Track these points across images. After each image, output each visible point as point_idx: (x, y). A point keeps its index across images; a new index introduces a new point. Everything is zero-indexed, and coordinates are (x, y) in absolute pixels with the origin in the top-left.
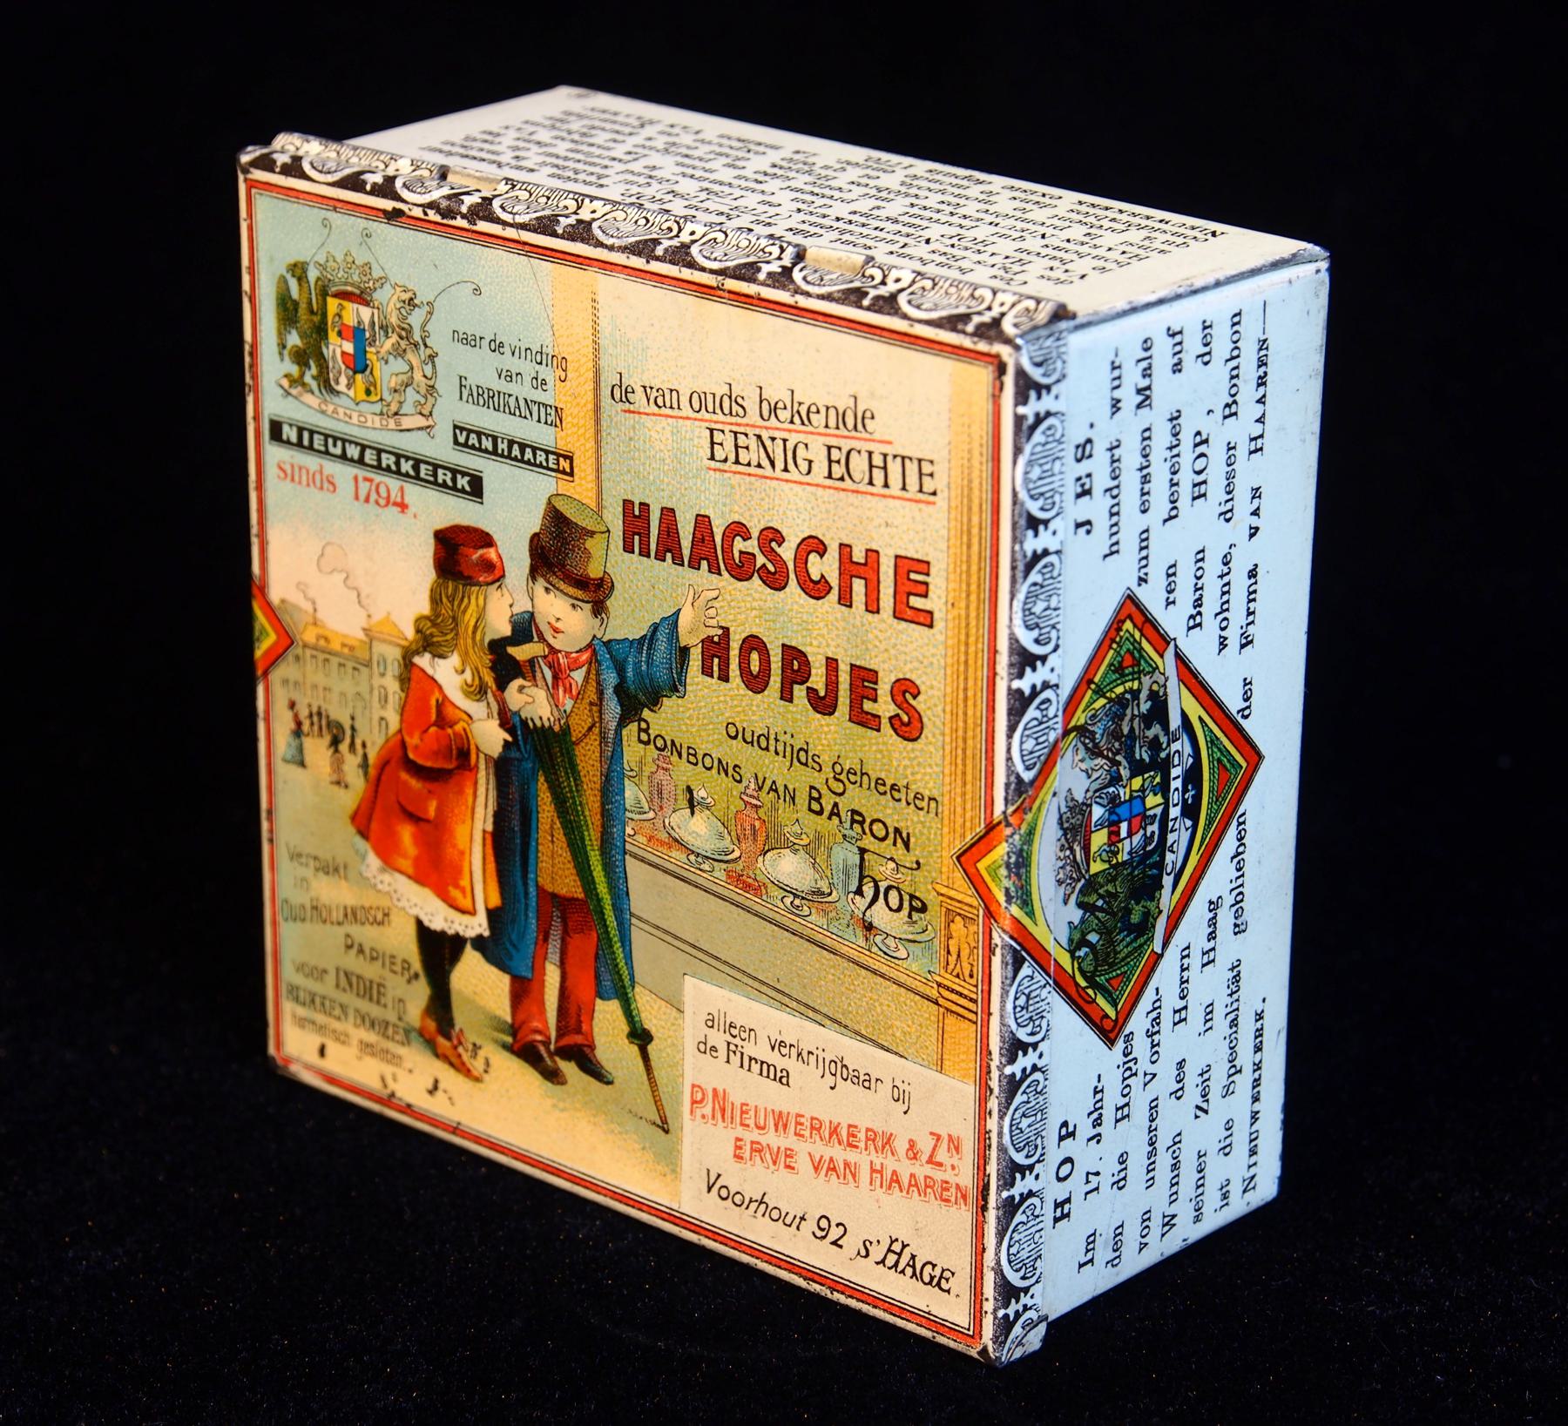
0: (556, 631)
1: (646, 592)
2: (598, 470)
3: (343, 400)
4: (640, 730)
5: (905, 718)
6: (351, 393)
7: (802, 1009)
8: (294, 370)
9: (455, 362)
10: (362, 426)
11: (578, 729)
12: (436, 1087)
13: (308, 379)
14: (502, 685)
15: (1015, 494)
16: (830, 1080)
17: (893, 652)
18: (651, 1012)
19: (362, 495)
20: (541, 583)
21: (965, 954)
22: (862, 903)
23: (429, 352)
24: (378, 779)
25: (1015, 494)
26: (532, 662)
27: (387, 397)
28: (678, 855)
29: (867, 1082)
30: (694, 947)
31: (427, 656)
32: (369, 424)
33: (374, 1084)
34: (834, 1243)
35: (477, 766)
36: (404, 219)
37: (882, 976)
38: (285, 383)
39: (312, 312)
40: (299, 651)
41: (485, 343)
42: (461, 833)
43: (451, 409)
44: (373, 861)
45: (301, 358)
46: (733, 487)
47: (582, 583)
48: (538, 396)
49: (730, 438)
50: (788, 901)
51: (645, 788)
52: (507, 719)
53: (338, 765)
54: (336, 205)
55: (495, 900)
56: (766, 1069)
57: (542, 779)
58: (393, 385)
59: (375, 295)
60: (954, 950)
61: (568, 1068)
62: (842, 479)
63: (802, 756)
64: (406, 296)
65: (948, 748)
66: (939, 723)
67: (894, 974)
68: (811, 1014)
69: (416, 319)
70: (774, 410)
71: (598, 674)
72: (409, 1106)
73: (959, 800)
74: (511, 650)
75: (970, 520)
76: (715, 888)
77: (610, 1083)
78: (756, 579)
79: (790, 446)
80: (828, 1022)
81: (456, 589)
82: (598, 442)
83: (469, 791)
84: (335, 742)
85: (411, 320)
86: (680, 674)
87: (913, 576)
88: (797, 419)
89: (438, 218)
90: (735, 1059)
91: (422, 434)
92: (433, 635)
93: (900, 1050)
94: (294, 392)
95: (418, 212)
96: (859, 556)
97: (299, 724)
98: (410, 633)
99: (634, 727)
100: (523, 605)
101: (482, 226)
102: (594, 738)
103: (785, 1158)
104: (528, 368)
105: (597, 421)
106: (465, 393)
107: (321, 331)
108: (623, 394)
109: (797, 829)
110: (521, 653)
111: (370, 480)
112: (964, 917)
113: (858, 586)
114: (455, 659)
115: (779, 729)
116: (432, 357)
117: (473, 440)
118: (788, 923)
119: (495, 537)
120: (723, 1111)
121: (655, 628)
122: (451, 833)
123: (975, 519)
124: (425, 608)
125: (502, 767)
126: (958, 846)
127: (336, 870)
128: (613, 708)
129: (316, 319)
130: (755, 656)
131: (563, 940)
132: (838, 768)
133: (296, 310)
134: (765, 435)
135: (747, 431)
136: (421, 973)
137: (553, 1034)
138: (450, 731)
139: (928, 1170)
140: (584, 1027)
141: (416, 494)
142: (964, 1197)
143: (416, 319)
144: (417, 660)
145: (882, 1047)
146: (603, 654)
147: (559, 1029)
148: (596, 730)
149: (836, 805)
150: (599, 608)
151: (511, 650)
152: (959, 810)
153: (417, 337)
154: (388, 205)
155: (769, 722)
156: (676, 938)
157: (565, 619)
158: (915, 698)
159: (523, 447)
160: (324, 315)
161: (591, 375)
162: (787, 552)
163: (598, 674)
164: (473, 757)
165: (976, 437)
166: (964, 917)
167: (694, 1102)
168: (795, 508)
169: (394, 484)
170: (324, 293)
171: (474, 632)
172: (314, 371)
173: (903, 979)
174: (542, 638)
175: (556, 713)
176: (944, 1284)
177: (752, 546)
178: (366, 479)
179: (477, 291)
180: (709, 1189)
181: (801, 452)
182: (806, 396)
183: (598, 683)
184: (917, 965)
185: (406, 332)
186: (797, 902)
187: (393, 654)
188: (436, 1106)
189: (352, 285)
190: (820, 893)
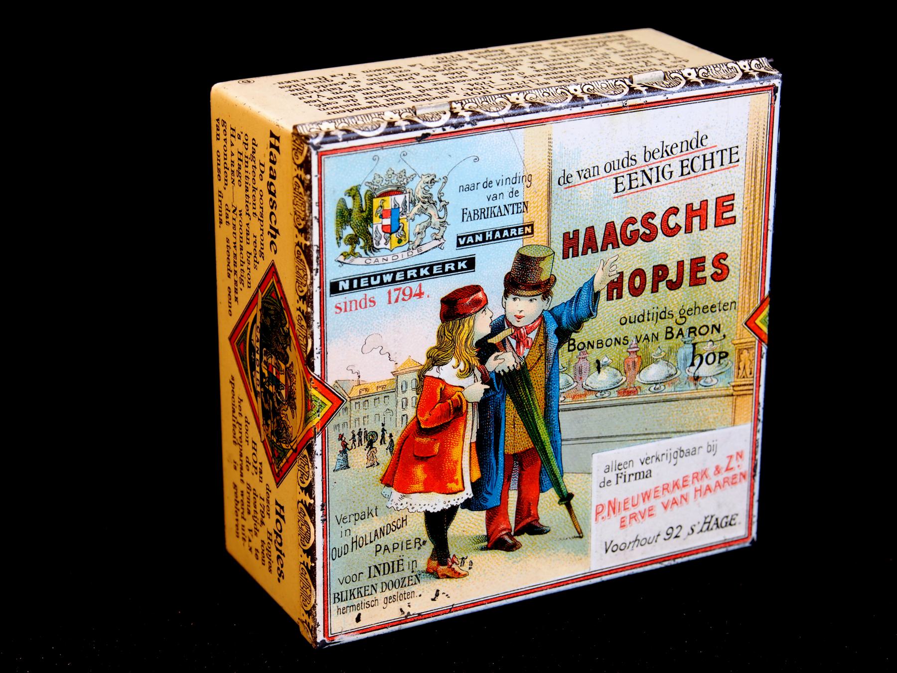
0: (519, 318)
1: (569, 276)
2: (549, 225)
3: (383, 252)
4: (569, 345)
5: (720, 271)
6: (388, 246)
7: (659, 436)
8: (348, 248)
9: (457, 201)
10: (394, 261)
11: (530, 363)
12: (437, 595)
13: (358, 249)
14: (483, 360)
15: (380, 135)
16: (674, 461)
17: (713, 244)
18: (570, 483)
19: (393, 299)
20: (511, 296)
21: (747, 367)
22: (693, 369)
23: (443, 203)
24: (400, 450)
25: (380, 135)
26: (503, 342)
27: (412, 239)
28: (591, 397)
29: (694, 452)
30: (598, 437)
31: (435, 368)
32: (400, 258)
33: (396, 615)
34: (676, 537)
35: (467, 412)
36: (430, 137)
37: (704, 398)
38: (342, 259)
39: (362, 211)
40: (347, 405)
41: (480, 186)
42: (455, 453)
43: (457, 227)
44: (396, 495)
46: (627, 201)
47: (537, 286)
48: (515, 200)
49: (627, 178)
50: (652, 389)
52: (485, 380)
54: (381, 146)
56: (639, 475)
58: (417, 230)
59: (407, 187)
60: (742, 367)
62: (689, 173)
63: (663, 315)
64: (429, 179)
65: (742, 276)
66: (737, 266)
67: (714, 393)
68: (664, 436)
69: (434, 190)
70: (652, 155)
71: (545, 328)
72: (419, 614)
73: (747, 296)
74: (489, 341)
75: (756, 166)
76: (614, 402)
78: (640, 241)
79: (660, 169)
80: (673, 435)
81: (454, 325)
82: (549, 210)
83: (461, 428)
84: (370, 444)
86: (593, 307)
87: (725, 204)
88: (665, 154)
89: (453, 129)
90: (621, 481)
92: (435, 360)
93: (712, 427)
94: (347, 261)
95: (440, 131)
96: (696, 206)
97: (345, 445)
98: (423, 360)
99: (566, 346)
100: (498, 313)
101: (481, 124)
102: (541, 364)
103: (650, 513)
104: (506, 189)
105: (549, 199)
106: (466, 217)
108: (566, 179)
109: (659, 351)
110: (494, 340)
111: (399, 289)
112: (747, 349)
113: (696, 221)
114: (454, 362)
115: (650, 308)
116: (444, 207)
117: (470, 239)
118: (656, 399)
120: (614, 509)
122: (449, 454)
123: (759, 165)
124: (434, 342)
125: (483, 406)
126: (746, 317)
127: (370, 513)
128: (553, 340)
129: (364, 214)
130: (638, 279)
131: (520, 475)
132: (682, 312)
133: (350, 215)
134: (647, 169)
135: (628, 173)
136: (428, 540)
137: (513, 526)
138: (449, 401)
139: (726, 474)
141: (428, 285)
142: (744, 477)
143: (434, 190)
144: (428, 373)
145: (703, 431)
146: (549, 318)
147: (516, 521)
148: (543, 358)
149: (681, 330)
150: (546, 295)
152: (747, 301)
153: (435, 198)
154: (419, 133)
155: (644, 307)
156: (588, 438)
157: (526, 309)
158: (725, 260)
159: (501, 231)
160: (371, 210)
161: (546, 177)
162: (657, 222)
163: (545, 328)
165: (762, 127)
166: (747, 349)
167: (597, 514)
168: (657, 200)
169: (414, 285)
170: (371, 198)
171: (466, 342)
172: (362, 243)
173: (718, 393)
174: (510, 325)
175: (518, 360)
176: (733, 522)
177: (638, 226)
178: (395, 290)
179: (477, 159)
180: (607, 551)
181: (667, 169)
182: (669, 142)
183: (545, 333)
184: (722, 384)
185: (428, 199)
186: (658, 386)
188: (442, 603)
189: (391, 186)
190: (671, 375)
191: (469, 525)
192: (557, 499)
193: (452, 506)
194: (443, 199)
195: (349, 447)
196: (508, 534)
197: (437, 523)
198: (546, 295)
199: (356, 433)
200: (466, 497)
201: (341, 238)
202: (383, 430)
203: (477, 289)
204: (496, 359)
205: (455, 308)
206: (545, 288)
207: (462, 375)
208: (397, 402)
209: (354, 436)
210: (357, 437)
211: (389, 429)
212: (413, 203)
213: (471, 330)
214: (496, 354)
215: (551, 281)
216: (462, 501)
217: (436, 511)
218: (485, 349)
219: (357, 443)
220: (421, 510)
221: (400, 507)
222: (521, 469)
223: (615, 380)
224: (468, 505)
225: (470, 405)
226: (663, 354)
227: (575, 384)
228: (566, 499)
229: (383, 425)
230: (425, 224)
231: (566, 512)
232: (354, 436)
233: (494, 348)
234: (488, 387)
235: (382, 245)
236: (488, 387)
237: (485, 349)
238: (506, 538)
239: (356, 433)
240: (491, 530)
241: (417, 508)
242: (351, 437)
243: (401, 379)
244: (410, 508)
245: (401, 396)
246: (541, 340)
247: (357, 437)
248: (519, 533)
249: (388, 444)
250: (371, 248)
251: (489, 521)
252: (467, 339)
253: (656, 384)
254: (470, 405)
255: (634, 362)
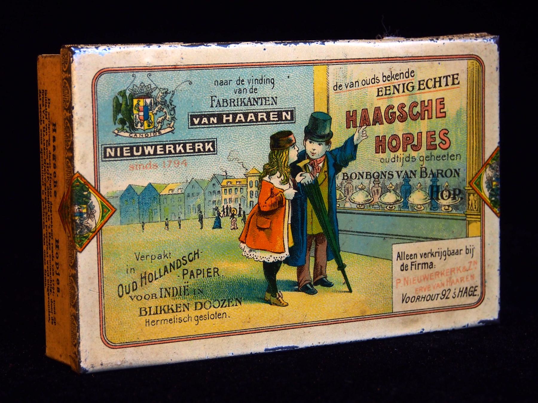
6: (143, 128)
8: (120, 126)
14: (294, 176)
23: (173, 106)
27: (156, 125)
32: (149, 136)
45: (123, 122)
47: (322, 137)
50: (388, 208)
51: (343, 191)
52: (296, 186)
53: (234, 223)
55: (291, 245)
57: (308, 201)
61: (318, 288)
69: (168, 98)
74: (298, 164)
77: (287, 305)
84: (233, 216)
85: (166, 98)
91: (170, 133)
92: (268, 171)
98: (261, 171)
100: (302, 148)
107: (130, 112)
109: (391, 185)
110: (301, 164)
114: (278, 174)
116: (173, 109)
119: (292, 131)
121: (346, 142)
124: (267, 161)
125: (294, 202)
129: (128, 107)
140: (324, 272)
143: (168, 98)
144: (264, 179)
146: (329, 156)
151: (298, 164)
153: (168, 103)
157: (316, 149)
164: (284, 202)
170: (132, 97)
171: (285, 163)
172: (128, 125)
174: (309, 158)
185: (164, 103)
187: (255, 179)
190: (398, 201)
191: (287, 274)
192: (336, 266)
193: (278, 260)
194: (172, 103)
195: (221, 215)
196: (310, 284)
197: (271, 269)
198: (328, 143)
199: (225, 207)
200: (286, 256)
201: (116, 120)
202: (240, 208)
203: (290, 133)
204: (301, 176)
205: (280, 142)
206: (327, 139)
207: (283, 183)
208: (247, 193)
209: (224, 209)
210: (225, 210)
211: (243, 209)
212: (156, 104)
213: (288, 156)
214: (301, 173)
215: (331, 135)
216: (283, 259)
217: (269, 262)
218: (295, 169)
219: (225, 214)
220: (262, 260)
221: (250, 257)
222: (316, 245)
223: (367, 198)
224: (287, 261)
225: (287, 201)
226: (393, 187)
227: (345, 198)
228: (341, 267)
229: (240, 205)
230: (163, 117)
231: (342, 275)
232: (224, 209)
233: (299, 170)
234: (296, 191)
235: (139, 127)
236: (296, 191)
237: (295, 169)
238: (308, 285)
239: (225, 207)
240: (301, 279)
241: (259, 258)
242: (222, 209)
243: (250, 179)
244: (255, 258)
245: (249, 190)
246: (325, 169)
247: (225, 210)
248: (316, 284)
249: (242, 216)
250: (133, 128)
251: (299, 273)
252: (285, 161)
253: (390, 205)
254: (287, 201)
255: (377, 190)
